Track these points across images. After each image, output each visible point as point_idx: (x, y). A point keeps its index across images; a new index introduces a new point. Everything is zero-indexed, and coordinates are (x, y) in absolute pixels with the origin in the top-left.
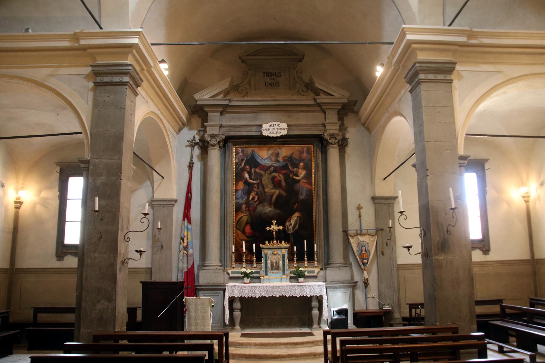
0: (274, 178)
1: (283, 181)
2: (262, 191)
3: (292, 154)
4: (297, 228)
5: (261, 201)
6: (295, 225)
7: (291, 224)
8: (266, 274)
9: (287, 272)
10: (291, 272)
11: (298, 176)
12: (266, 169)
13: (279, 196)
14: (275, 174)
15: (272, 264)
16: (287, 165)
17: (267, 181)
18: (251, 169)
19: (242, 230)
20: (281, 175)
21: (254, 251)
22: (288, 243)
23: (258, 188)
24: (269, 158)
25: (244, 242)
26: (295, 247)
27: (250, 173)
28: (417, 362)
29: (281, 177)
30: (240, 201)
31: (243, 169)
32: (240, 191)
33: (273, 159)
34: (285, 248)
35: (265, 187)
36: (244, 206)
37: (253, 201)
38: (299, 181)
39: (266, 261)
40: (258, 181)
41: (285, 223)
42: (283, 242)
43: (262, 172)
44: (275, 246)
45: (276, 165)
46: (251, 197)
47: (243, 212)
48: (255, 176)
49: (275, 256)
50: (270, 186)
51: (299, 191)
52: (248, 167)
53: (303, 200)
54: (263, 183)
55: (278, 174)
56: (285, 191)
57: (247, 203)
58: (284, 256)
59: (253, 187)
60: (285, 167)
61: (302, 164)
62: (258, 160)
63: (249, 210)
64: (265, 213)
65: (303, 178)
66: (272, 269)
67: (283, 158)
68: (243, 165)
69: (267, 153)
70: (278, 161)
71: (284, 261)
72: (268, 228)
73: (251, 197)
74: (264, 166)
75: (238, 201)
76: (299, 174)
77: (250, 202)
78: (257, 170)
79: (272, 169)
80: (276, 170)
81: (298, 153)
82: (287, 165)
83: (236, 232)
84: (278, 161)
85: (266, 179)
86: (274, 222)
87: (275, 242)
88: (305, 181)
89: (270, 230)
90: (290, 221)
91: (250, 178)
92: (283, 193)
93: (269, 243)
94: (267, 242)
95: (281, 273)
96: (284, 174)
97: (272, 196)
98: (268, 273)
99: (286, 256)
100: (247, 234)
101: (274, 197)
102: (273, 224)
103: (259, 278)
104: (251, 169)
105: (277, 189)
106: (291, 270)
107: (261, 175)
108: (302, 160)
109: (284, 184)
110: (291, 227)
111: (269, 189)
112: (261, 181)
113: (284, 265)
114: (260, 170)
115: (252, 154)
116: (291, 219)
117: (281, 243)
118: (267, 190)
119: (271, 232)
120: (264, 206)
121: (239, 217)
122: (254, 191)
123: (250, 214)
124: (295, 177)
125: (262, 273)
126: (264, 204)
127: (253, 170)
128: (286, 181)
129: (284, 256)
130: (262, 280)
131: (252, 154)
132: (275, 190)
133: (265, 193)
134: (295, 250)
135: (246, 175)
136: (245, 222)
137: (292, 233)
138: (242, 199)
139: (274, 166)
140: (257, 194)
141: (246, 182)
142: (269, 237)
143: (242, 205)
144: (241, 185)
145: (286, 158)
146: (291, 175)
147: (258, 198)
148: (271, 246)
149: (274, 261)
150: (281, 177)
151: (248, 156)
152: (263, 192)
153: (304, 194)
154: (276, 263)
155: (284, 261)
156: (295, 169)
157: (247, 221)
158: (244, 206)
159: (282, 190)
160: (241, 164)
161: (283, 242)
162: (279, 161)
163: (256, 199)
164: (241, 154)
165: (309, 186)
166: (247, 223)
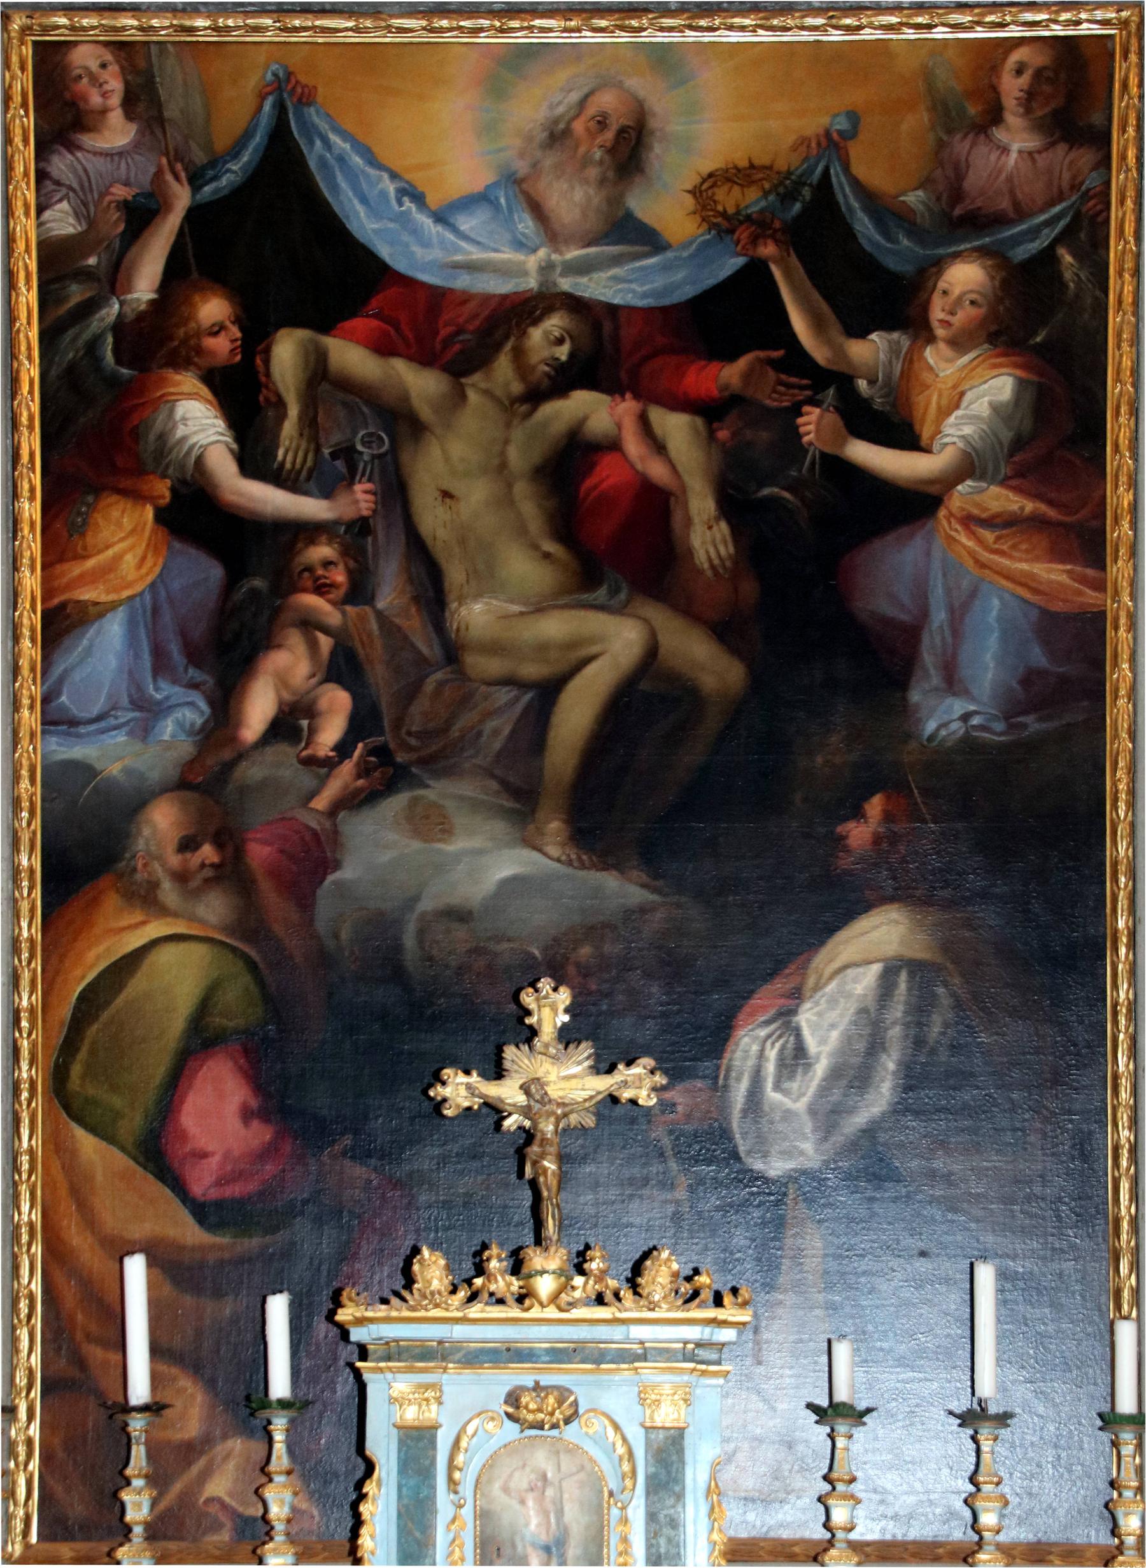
0: (572, 457)
1: (701, 504)
2: (416, 627)
3: (833, 145)
5: (389, 762)
6: (853, 1075)
7: (796, 1058)
11: (902, 434)
12: (461, 334)
13: (645, 701)
14: (591, 409)
16: (753, 282)
17: (476, 495)
18: (256, 337)
19: (133, 1123)
20: (677, 427)
21: (280, 1385)
23: (359, 591)
24: (521, 191)
25: (136, 1269)
27: (242, 397)
28: (1081, 1564)
29: (674, 449)
30: (113, 754)
31: (154, 341)
32: (112, 633)
33: (572, 198)
35: (455, 574)
36: (163, 821)
37: (284, 752)
38: (916, 505)
40: (361, 498)
41: (717, 1037)
43: (421, 384)
45: (621, 284)
46: (259, 708)
47: (147, 899)
48: (310, 423)
50: (526, 568)
51: (912, 633)
52: (213, 309)
53: (969, 745)
54: (432, 519)
55: (628, 407)
56: (725, 632)
57: (209, 776)
59: (286, 581)
60: (733, 315)
61: (965, 276)
62: (365, 225)
63: (232, 873)
64: (458, 915)
65: (970, 466)
67: (703, 192)
68: (144, 287)
69: (488, 129)
70: (628, 233)
73: (259, 708)
74: (437, 297)
75: (78, 751)
76: (927, 403)
77: (252, 772)
78: (350, 356)
79: (548, 340)
80: (608, 350)
81: (916, 122)
82: (753, 282)
83: (56, 1144)
84: (628, 233)
85: (467, 476)
86: (550, 1007)
88: (1000, 499)
90: (786, 1015)
91: (254, 459)
92: (706, 661)
96: (710, 411)
97: (549, 691)
100: (203, 1181)
101: (576, 715)
104: (256, 337)
105: (619, 611)
107: (401, 423)
108: (963, 221)
109: (707, 538)
110: (793, 1100)
111: (510, 602)
112: (396, 491)
114: (383, 348)
115: (280, 134)
116: (797, 995)
118: (475, 615)
120: (430, 824)
121: (94, 959)
122: (309, 625)
123: (249, 926)
124: (866, 454)
126: (436, 791)
127: (286, 352)
128: (733, 503)
131: (280, 134)
132: (594, 622)
133: (452, 652)
135: (197, 422)
136: (177, 1024)
138: (144, 731)
139: (575, 304)
140: (344, 667)
141: (194, 515)
143: (132, 804)
144: (126, 543)
145: (751, 199)
146: (814, 424)
147: (362, 723)
149: (530, 1523)
150: (674, 449)
151: (216, 162)
152: (425, 644)
153: (988, 664)
156: (871, 351)
157: (204, 1007)
158: (163, 821)
159: (688, 611)
160: (115, 279)
162: (646, 239)
163: (330, 733)
164: (117, 133)
165: (1054, 573)
166: (202, 1038)
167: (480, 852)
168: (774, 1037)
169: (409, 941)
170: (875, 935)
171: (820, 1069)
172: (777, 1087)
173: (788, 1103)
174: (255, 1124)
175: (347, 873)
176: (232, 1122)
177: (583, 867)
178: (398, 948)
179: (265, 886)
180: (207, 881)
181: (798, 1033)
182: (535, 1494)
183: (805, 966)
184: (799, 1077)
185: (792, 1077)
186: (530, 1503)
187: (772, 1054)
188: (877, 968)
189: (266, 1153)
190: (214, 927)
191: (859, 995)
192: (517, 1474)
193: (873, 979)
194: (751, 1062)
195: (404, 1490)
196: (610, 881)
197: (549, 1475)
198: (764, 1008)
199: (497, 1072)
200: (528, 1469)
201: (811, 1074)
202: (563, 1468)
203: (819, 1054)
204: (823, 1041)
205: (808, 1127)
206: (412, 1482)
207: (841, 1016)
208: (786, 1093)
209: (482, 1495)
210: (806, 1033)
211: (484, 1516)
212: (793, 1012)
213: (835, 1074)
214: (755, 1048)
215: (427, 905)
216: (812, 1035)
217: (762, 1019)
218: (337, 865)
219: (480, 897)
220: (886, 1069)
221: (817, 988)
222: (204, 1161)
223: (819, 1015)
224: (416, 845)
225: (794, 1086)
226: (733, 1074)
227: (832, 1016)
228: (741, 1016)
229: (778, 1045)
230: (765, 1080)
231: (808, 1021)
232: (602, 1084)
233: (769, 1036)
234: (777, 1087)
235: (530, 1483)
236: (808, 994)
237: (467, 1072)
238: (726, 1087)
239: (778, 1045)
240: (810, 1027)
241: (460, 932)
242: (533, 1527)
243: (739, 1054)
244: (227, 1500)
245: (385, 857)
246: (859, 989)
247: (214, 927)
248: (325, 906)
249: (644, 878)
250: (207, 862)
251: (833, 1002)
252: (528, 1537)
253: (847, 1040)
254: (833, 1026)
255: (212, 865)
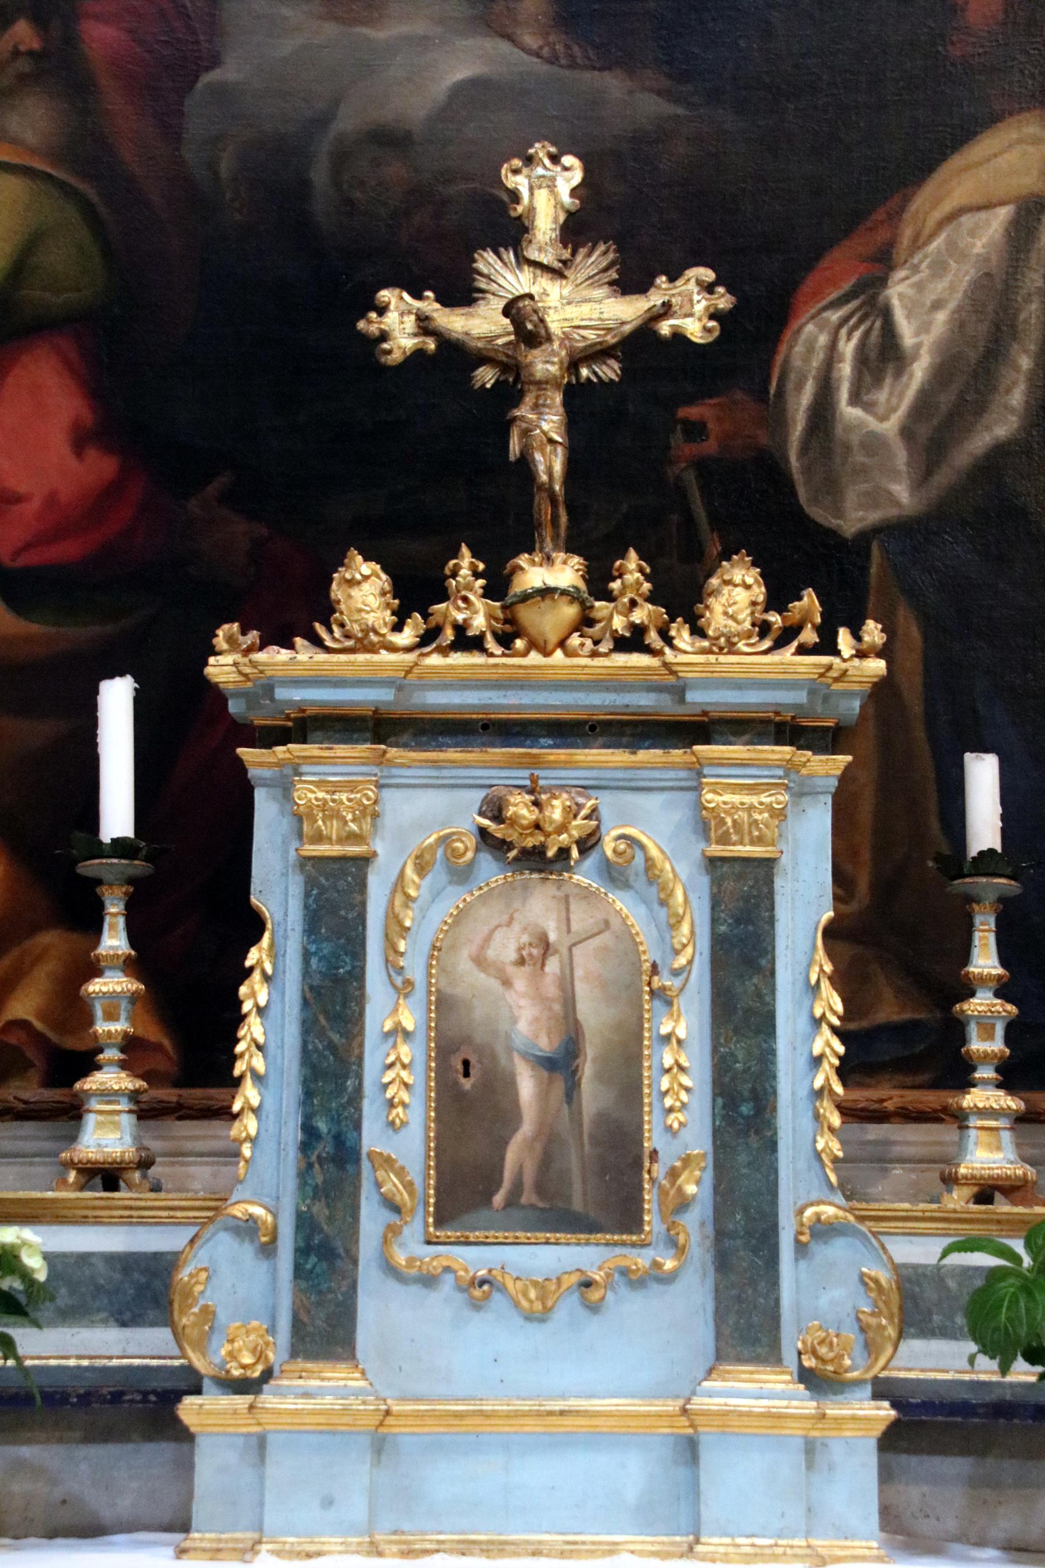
4: (1002, 423)
7: (884, 355)
8: (325, 1328)
9: (822, 1292)
10: (915, 1306)
15: (467, 1088)
21: (117, 815)
22: (844, 612)
26: (983, 776)
34: (786, 730)
39: (333, 1004)
42: (736, 592)
44: (566, 671)
49: (540, 906)
53: (864, 624)
58: (743, 899)
64: (389, 139)
66: (464, 1191)
71: (742, 1012)
72: (399, 322)
87: (551, 571)
89: (454, 356)
90: (868, 295)
93: (416, 591)
94: (364, 590)
95: (689, 1301)
98: (381, 1310)
99: (804, 902)
102: (510, 232)
103: (146, 1410)
106: (920, 1251)
110: (877, 419)
113: (743, 1103)
116: (883, 262)
117: (681, 597)
119: (468, 397)
125: (237, 1291)
129: (743, 899)
130: (213, 1465)
134: (985, 825)
137: (897, 531)
142: (434, 480)
148: (451, 682)
149: (522, 1020)
154: (561, 1064)
155: (742, 1012)
161: (736, 592)
167: (423, 42)
168: (852, 322)
169: (320, 175)
170: (1002, 162)
171: (919, 371)
172: (855, 399)
173: (872, 423)
174: (92, 454)
175: (230, 71)
176: (59, 445)
177: (573, 65)
178: (305, 184)
179: (113, 98)
180: (22, 78)
181: (887, 314)
182: (527, 969)
183: (895, 217)
184: (888, 381)
185: (878, 381)
186: (520, 984)
187: (848, 348)
188: (1004, 213)
189: (110, 493)
190: (33, 151)
191: (978, 255)
192: (498, 935)
193: (1001, 230)
194: (817, 361)
195: (314, 961)
196: (613, 84)
197: (552, 937)
198: (833, 282)
199: (461, 292)
200: (516, 927)
201: (905, 379)
202: (574, 927)
203: (918, 346)
204: (924, 328)
205: (901, 456)
206: (327, 948)
207: (952, 288)
208: (869, 407)
209: (443, 970)
210: (899, 315)
211: (443, 1005)
212: (882, 282)
213: (942, 374)
214: (823, 339)
215: (348, 121)
216: (908, 317)
217: (834, 296)
218: (215, 61)
219: (422, 113)
220: (1017, 369)
221: (918, 244)
222: (16, 508)
223: (920, 287)
224: (331, 29)
225: (882, 396)
226: (792, 376)
227: (940, 287)
228: (808, 285)
229: (857, 335)
230: (838, 389)
231: (901, 296)
232: (626, 311)
233: (845, 320)
234: (855, 399)
235: (520, 949)
236: (903, 258)
237: (418, 296)
238: (780, 393)
239: (857, 335)
240: (904, 306)
241: (395, 170)
242: (523, 1026)
243: (799, 349)
244: (38, 1025)
245: (287, 47)
246: (979, 246)
247: (33, 151)
248: (198, 119)
249: (665, 83)
250: (22, 48)
251: (939, 268)
252: (518, 1042)
253: (959, 325)
254: (937, 305)
255: (31, 53)
